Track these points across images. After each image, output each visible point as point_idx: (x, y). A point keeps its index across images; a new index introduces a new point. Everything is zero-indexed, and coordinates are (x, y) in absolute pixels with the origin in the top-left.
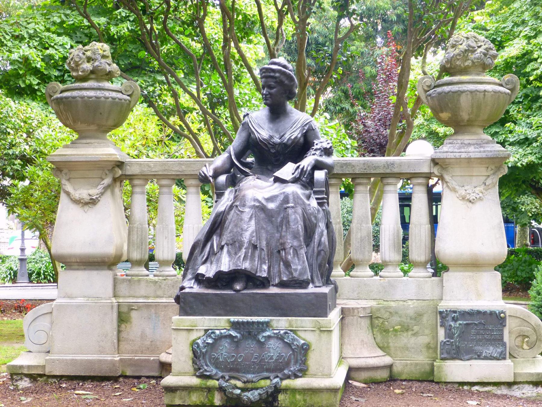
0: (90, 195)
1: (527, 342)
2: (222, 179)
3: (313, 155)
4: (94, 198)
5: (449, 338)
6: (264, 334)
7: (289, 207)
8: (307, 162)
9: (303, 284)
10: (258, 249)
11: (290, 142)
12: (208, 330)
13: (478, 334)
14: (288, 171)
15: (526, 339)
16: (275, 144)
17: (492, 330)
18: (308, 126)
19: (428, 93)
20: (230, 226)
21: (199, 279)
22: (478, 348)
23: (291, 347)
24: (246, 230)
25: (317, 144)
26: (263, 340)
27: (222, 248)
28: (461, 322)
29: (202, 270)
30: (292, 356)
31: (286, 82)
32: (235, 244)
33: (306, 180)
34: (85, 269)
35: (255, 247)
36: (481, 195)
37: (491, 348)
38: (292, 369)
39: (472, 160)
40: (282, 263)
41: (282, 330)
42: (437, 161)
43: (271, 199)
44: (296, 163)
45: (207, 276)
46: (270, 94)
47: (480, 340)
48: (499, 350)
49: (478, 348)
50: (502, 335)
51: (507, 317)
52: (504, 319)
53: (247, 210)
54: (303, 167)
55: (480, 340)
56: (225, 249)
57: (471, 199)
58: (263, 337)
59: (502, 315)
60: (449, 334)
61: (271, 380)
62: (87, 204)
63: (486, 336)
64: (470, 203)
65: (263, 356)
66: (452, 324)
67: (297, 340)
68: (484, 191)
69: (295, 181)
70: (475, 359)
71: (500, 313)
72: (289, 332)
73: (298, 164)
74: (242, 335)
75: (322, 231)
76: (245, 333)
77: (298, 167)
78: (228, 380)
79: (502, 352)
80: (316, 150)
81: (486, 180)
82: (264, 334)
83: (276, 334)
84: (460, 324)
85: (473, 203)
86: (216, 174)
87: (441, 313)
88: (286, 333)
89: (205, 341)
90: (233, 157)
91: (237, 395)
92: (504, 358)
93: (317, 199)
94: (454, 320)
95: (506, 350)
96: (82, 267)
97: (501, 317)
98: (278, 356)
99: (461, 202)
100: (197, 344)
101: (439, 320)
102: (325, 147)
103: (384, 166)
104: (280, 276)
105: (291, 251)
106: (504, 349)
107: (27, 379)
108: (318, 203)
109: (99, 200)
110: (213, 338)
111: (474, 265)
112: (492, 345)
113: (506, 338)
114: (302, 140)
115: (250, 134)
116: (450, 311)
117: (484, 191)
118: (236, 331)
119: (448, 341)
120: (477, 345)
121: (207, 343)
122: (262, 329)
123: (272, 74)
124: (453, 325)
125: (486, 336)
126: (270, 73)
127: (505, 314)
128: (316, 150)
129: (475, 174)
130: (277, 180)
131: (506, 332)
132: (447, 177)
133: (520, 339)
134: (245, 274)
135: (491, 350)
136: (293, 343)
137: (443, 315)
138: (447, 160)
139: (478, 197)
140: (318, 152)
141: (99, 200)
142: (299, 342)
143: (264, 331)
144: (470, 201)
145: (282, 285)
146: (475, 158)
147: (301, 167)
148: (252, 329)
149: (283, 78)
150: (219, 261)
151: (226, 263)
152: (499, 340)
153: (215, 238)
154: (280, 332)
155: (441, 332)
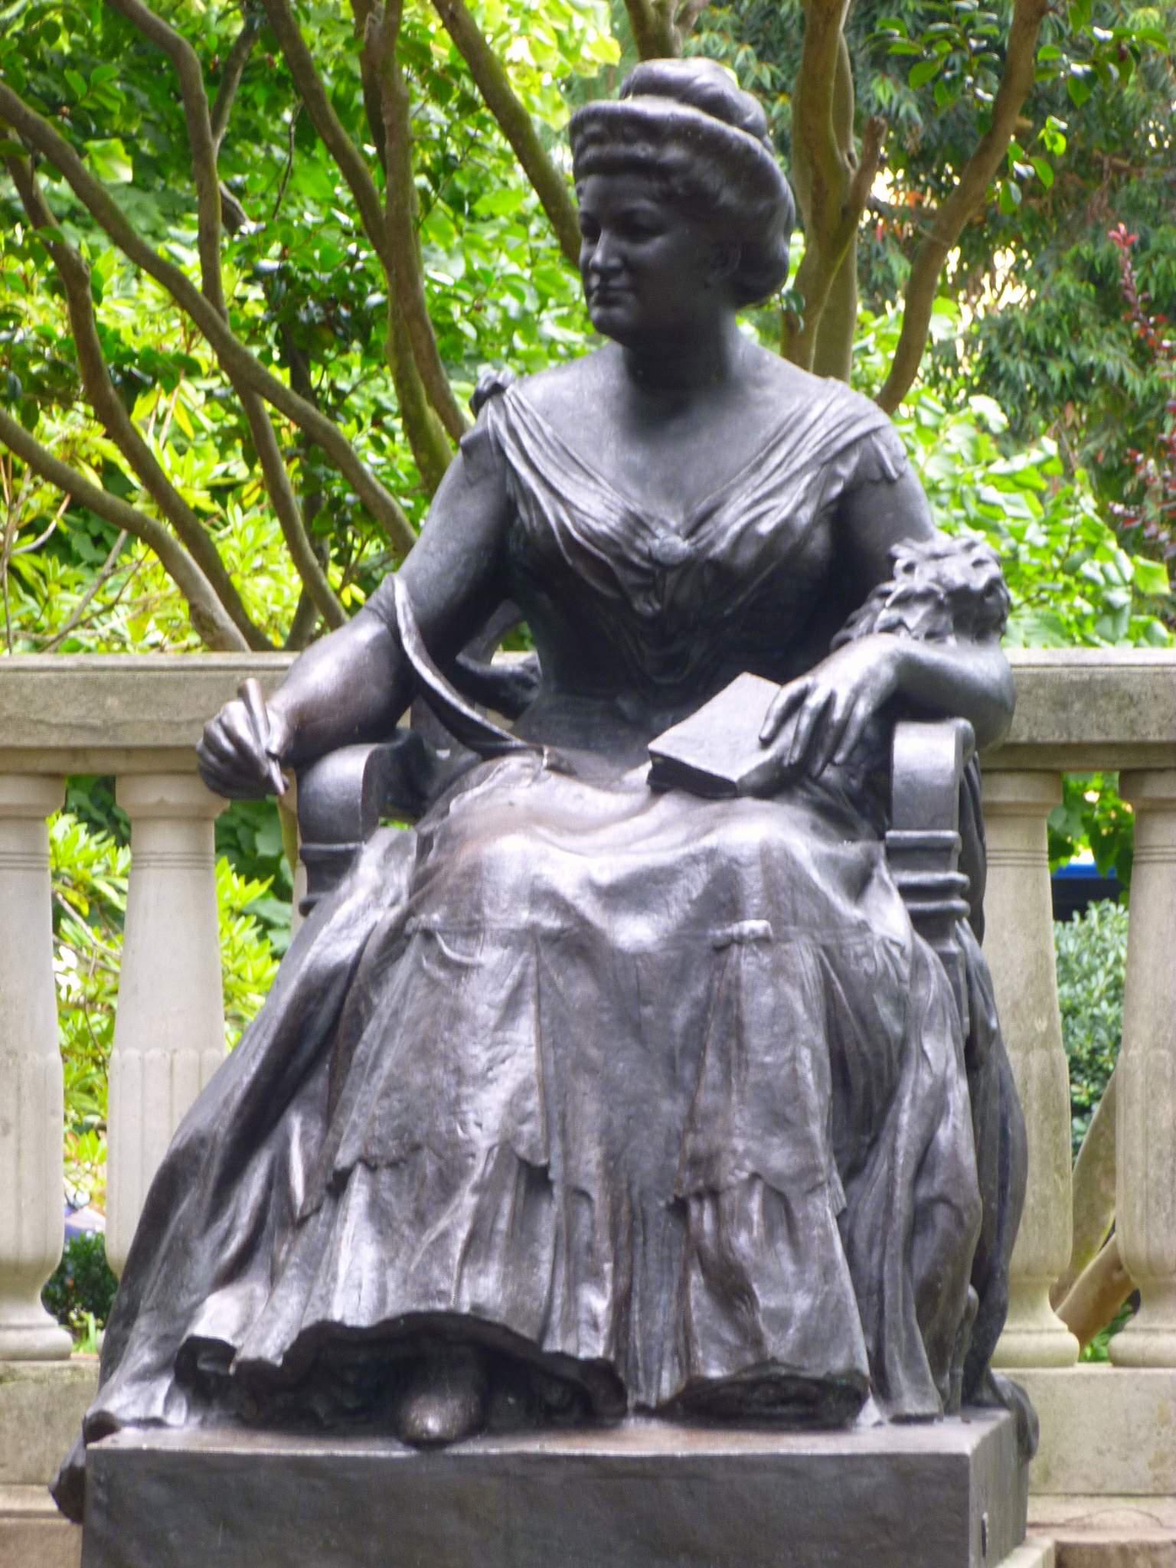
2: (345, 769)
3: (890, 628)
10: (557, 1191)
11: (748, 554)
14: (734, 724)
16: (658, 568)
18: (854, 459)
20: (384, 1052)
25: (909, 568)
27: (337, 1185)
31: (728, 196)
32: (416, 1166)
40: (696, 1278)
44: (782, 677)
45: (248, 1351)
46: (629, 266)
53: (489, 956)
56: (358, 1195)
69: (776, 784)
73: (794, 687)
75: (941, 1089)
77: (796, 704)
80: (905, 600)
86: (308, 743)
90: (409, 644)
93: (908, 892)
102: (959, 580)
104: (685, 1358)
105: (755, 1205)
108: (920, 922)
115: (510, 504)
123: (643, 150)
126: (629, 140)
130: (674, 778)
140: (915, 617)
145: (700, 1406)
149: (710, 176)
150: (318, 1264)
151: (357, 1280)
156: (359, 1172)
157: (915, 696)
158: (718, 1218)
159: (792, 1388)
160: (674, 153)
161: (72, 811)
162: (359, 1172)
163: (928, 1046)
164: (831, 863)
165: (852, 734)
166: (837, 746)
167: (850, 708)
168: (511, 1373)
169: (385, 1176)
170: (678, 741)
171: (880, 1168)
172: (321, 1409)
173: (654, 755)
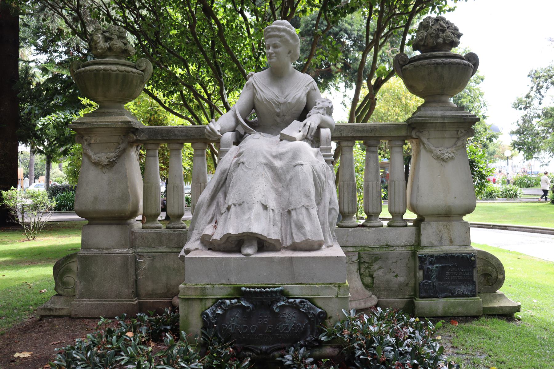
0: (108, 158)
4: (111, 160)
5: (427, 279)
6: (279, 304)
9: (317, 246)
11: (294, 101)
12: (218, 299)
14: (295, 129)
18: (310, 86)
19: (404, 67)
22: (451, 287)
23: (308, 316)
26: (277, 311)
29: (208, 230)
35: (265, 207)
36: (453, 154)
37: (463, 287)
38: (308, 339)
41: (298, 298)
45: (214, 237)
46: (276, 53)
48: (470, 289)
49: (451, 287)
51: (477, 259)
52: (474, 262)
58: (278, 307)
59: (473, 258)
60: (427, 276)
65: (278, 327)
66: (430, 267)
67: (313, 309)
68: (455, 151)
72: (304, 300)
74: (255, 306)
76: (258, 303)
77: (305, 125)
79: (472, 290)
80: (319, 109)
82: (279, 304)
83: (291, 303)
84: (436, 267)
85: (446, 161)
87: (420, 258)
88: (301, 302)
89: (215, 311)
93: (324, 156)
94: (431, 263)
97: (471, 260)
98: (293, 327)
99: (436, 161)
100: (207, 314)
101: (418, 264)
108: (326, 161)
110: (223, 309)
113: (476, 279)
114: (305, 100)
116: (428, 256)
117: (455, 151)
118: (247, 301)
119: (426, 282)
121: (217, 314)
123: (277, 33)
126: (274, 31)
128: (319, 109)
132: (425, 140)
134: (257, 237)
135: (462, 289)
136: (309, 313)
139: (450, 156)
140: (321, 111)
142: (316, 311)
143: (278, 300)
152: (470, 280)
153: (220, 195)
154: (295, 301)
155: (420, 274)
156: (233, 206)
160: (282, 33)
161: (327, 83)
168: (262, 244)
170: (285, 131)
171: (322, 204)
173: (281, 134)
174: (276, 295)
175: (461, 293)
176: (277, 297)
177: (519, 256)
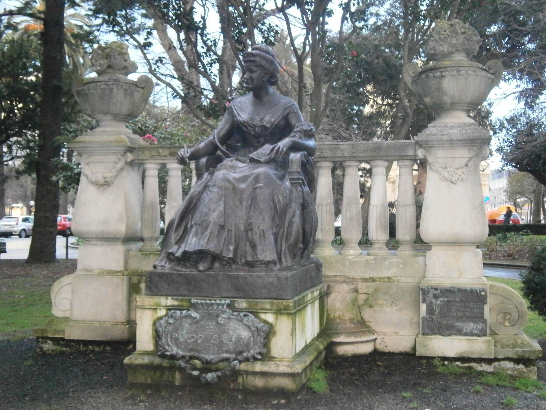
0: (105, 178)
1: (509, 319)
3: (293, 137)
4: (108, 180)
7: (258, 187)
8: (284, 143)
10: (226, 230)
13: (459, 311)
15: (508, 317)
17: (473, 308)
21: (170, 257)
22: (459, 324)
24: (214, 211)
25: (298, 127)
28: (442, 300)
30: (252, 339)
32: (204, 226)
33: (280, 162)
34: (102, 245)
39: (455, 142)
40: (248, 244)
42: (420, 143)
43: (244, 179)
44: (272, 144)
47: (462, 318)
48: (479, 327)
49: (459, 324)
50: (482, 313)
51: (488, 294)
54: (279, 148)
55: (462, 318)
57: (453, 180)
59: (483, 293)
60: (430, 310)
61: (230, 362)
62: (102, 185)
63: (466, 313)
64: (453, 185)
70: (456, 335)
71: (480, 292)
73: (274, 145)
75: (294, 213)
77: (273, 148)
78: (188, 360)
79: (482, 329)
80: (295, 132)
81: (468, 161)
84: (441, 301)
85: (455, 184)
90: (216, 140)
91: (196, 376)
92: (485, 335)
93: (290, 179)
95: (486, 327)
96: (99, 243)
97: (482, 295)
101: (421, 297)
102: (305, 129)
103: (372, 150)
104: (246, 257)
106: (484, 326)
107: (50, 342)
108: (292, 184)
109: (113, 183)
111: (456, 243)
112: (472, 322)
120: (458, 321)
122: (221, 310)
123: (252, 59)
124: (434, 301)
125: (466, 313)
127: (485, 292)
129: (457, 156)
130: (252, 160)
131: (487, 308)
133: (501, 316)
135: (471, 326)
137: (425, 292)
138: (430, 143)
141: (113, 183)
144: (453, 183)
146: (456, 140)
147: (276, 148)
148: (212, 310)
149: (263, 63)
151: (192, 243)
156: (194, 225)
157: (295, 147)
158: (252, 235)
159: (263, 262)
162: (194, 225)
163: (292, 205)
164: (276, 174)
165: (283, 153)
166: (280, 155)
167: (283, 149)
169: (198, 226)
170: (254, 155)
172: (188, 265)
174: (223, 307)
175: (469, 331)
176: (224, 310)
177: (357, 250)
